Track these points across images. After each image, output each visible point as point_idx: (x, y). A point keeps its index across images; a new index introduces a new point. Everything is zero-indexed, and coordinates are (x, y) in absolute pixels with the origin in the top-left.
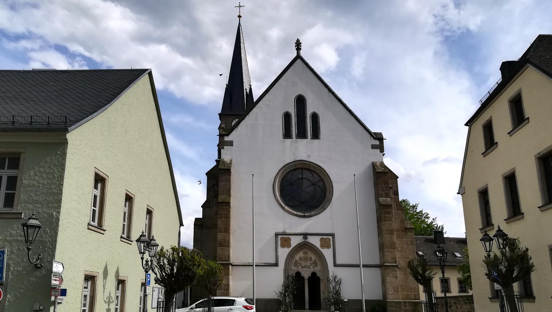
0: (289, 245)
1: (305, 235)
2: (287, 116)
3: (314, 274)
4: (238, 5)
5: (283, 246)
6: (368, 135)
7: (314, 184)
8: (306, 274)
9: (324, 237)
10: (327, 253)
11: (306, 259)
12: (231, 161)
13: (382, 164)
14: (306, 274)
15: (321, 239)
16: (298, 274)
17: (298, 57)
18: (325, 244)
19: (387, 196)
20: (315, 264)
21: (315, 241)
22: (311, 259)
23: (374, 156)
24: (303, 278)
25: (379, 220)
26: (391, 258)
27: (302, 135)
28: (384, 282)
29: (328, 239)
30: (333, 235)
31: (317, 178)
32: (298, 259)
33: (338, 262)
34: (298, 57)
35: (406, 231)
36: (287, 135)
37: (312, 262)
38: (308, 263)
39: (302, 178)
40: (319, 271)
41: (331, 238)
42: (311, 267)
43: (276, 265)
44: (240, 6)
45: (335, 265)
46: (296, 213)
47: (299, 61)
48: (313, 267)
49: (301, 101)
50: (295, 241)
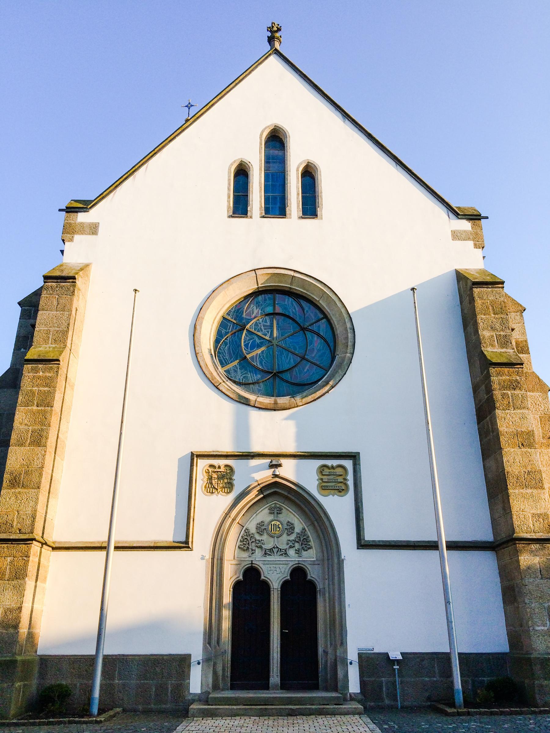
2: (242, 173)
3: (298, 572)
5: (211, 488)
8: (275, 574)
10: (338, 509)
14: (275, 574)
22: (290, 528)
24: (265, 586)
27: (276, 207)
29: (341, 468)
30: (354, 457)
31: (311, 314)
33: (369, 536)
36: (240, 207)
37: (293, 537)
41: (348, 464)
42: (292, 552)
43: (185, 545)
48: (298, 552)
49: (276, 140)
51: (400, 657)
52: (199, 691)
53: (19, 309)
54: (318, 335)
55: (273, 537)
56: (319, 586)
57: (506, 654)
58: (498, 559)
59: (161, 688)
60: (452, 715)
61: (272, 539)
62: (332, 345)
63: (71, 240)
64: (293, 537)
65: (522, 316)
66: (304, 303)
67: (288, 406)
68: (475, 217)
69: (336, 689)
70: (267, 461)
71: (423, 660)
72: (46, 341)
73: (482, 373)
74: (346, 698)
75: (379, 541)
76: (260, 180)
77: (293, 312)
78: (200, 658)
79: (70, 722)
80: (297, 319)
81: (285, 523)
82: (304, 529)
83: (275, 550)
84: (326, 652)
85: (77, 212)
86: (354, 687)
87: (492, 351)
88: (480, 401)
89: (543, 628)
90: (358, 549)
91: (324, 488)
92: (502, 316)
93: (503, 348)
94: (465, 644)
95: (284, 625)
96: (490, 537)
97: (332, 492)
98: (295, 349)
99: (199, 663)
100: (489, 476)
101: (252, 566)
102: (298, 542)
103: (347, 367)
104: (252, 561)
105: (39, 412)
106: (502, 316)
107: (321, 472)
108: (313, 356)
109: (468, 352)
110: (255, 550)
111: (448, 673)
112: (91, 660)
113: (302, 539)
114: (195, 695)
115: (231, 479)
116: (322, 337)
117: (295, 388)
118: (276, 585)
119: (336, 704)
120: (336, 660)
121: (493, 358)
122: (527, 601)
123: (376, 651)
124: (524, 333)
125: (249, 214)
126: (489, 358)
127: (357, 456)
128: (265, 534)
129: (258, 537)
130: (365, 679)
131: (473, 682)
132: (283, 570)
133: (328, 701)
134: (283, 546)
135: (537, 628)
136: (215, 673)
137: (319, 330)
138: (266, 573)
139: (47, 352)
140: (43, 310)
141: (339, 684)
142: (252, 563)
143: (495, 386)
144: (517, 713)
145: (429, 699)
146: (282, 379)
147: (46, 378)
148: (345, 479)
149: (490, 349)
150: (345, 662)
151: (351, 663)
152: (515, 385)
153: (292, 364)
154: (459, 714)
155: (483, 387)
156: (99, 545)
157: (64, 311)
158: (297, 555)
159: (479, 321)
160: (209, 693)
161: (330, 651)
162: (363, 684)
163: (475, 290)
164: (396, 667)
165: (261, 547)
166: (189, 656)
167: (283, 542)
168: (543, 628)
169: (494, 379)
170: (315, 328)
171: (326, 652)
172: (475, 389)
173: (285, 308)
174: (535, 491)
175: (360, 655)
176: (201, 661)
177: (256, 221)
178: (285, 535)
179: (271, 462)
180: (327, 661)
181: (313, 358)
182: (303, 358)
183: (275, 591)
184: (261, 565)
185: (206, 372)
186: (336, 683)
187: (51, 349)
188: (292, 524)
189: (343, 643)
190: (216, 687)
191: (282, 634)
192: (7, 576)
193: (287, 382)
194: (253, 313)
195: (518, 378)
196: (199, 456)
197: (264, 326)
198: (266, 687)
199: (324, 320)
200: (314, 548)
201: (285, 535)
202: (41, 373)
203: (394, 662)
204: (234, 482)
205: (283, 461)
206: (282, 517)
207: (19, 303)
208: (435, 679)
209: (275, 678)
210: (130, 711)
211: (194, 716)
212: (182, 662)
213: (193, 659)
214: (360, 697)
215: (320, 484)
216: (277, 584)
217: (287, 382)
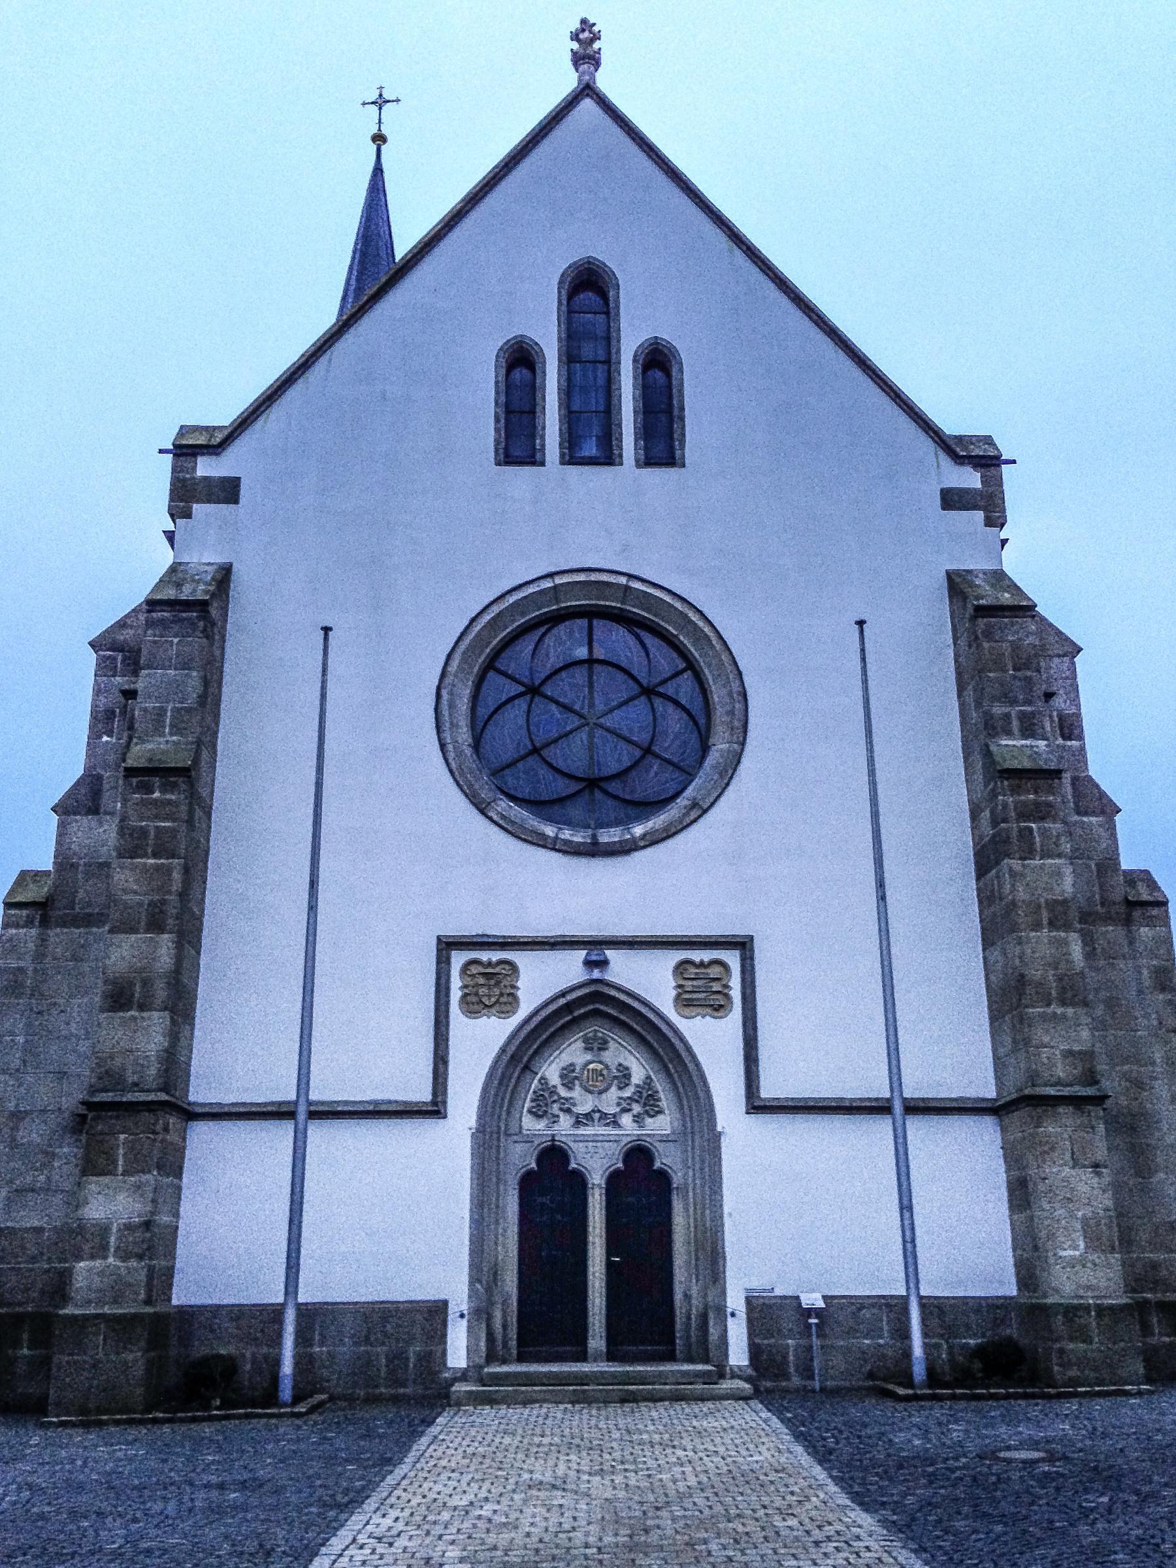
0: (507, 1002)
1: (596, 948)
2: (520, 358)
3: (638, 1156)
4: (374, 97)
5: (474, 1005)
6: (926, 446)
7: (649, 692)
8: (596, 1160)
9: (697, 956)
10: (712, 1041)
11: (598, 1082)
12: (224, 575)
13: (999, 578)
14: (596, 1160)
15: (681, 968)
16: (554, 1156)
17: (587, 90)
18: (701, 993)
19: (1029, 729)
20: (648, 1101)
21: (651, 980)
22: (624, 1076)
23: (960, 543)
24: (578, 1181)
25: (987, 858)
26: (1069, 1054)
27: (591, 443)
28: (1021, 1194)
29: (718, 967)
30: (744, 945)
31: (665, 660)
32: (554, 1079)
33: (768, 1090)
34: (587, 90)
35: (1128, 922)
36: (517, 444)
37: (628, 1093)
38: (610, 1101)
39: (591, 662)
40: (665, 1140)
41: (732, 959)
42: (626, 1120)
43: (435, 1110)
44: (381, 102)
45: (756, 1105)
46: (550, 831)
47: (587, 104)
48: (638, 1119)
49: (589, 286)
50: (541, 980)
51: (821, 1304)
52: (463, 1364)
53: (92, 657)
54: (677, 703)
55: (591, 1092)
56: (677, 1179)
57: (1011, 1298)
58: (1004, 1130)
59: (397, 1358)
60: (907, 1399)
61: (590, 1096)
62: (702, 721)
64: (628, 1093)
66: (649, 639)
69: (706, 1361)
70: (582, 954)
71: (860, 1309)
72: (158, 730)
73: (986, 786)
74: (721, 1372)
75: (787, 1099)
78: (464, 1307)
79: (247, 1416)
80: (635, 672)
82: (648, 1077)
84: (687, 1297)
86: (738, 1355)
88: (981, 837)
89: (1071, 1253)
90: (747, 1113)
91: (685, 1002)
92: (1029, 673)
95: (612, 1246)
96: (990, 1092)
97: (699, 1010)
99: (462, 1316)
100: (993, 978)
101: (553, 1145)
102: (637, 1101)
103: (730, 772)
104: (553, 1136)
105: (157, 868)
106: (1029, 673)
108: (668, 747)
110: (558, 1116)
111: (904, 1334)
112: (275, 1314)
113: (645, 1095)
116: (684, 708)
117: (631, 811)
118: (597, 1179)
119: (705, 1383)
124: (1076, 701)
125: (538, 456)
127: (748, 946)
128: (577, 1088)
129: (563, 1092)
130: (757, 1341)
131: (950, 1347)
135: (1064, 1253)
137: (677, 693)
138: (579, 1156)
142: (553, 1140)
144: (1017, 1396)
145: (871, 1375)
146: (606, 792)
148: (726, 986)
150: (721, 1311)
151: (733, 1315)
153: (627, 763)
154: (916, 1398)
155: (987, 813)
158: (635, 1125)
160: (481, 1367)
161: (694, 1291)
162: (755, 1352)
164: (813, 1321)
165: (568, 1111)
166: (445, 1303)
167: (610, 1101)
168: (1071, 1253)
170: (669, 689)
171: (687, 1297)
175: (749, 1301)
176: (465, 1312)
177: (555, 481)
178: (614, 1089)
181: (666, 749)
183: (597, 1192)
184: (572, 1144)
186: (707, 1348)
188: (627, 1069)
191: (610, 1265)
192: (120, 1169)
193: (616, 797)
198: (582, 1357)
199: (688, 675)
200: (667, 1112)
203: (809, 1312)
204: (520, 994)
206: (607, 1056)
207: (92, 644)
208: (881, 1341)
209: (597, 1341)
210: (344, 1398)
211: (459, 1404)
212: (435, 1314)
213: (453, 1310)
214: (750, 1371)
215: (678, 996)
216: (599, 1177)
217: (616, 797)
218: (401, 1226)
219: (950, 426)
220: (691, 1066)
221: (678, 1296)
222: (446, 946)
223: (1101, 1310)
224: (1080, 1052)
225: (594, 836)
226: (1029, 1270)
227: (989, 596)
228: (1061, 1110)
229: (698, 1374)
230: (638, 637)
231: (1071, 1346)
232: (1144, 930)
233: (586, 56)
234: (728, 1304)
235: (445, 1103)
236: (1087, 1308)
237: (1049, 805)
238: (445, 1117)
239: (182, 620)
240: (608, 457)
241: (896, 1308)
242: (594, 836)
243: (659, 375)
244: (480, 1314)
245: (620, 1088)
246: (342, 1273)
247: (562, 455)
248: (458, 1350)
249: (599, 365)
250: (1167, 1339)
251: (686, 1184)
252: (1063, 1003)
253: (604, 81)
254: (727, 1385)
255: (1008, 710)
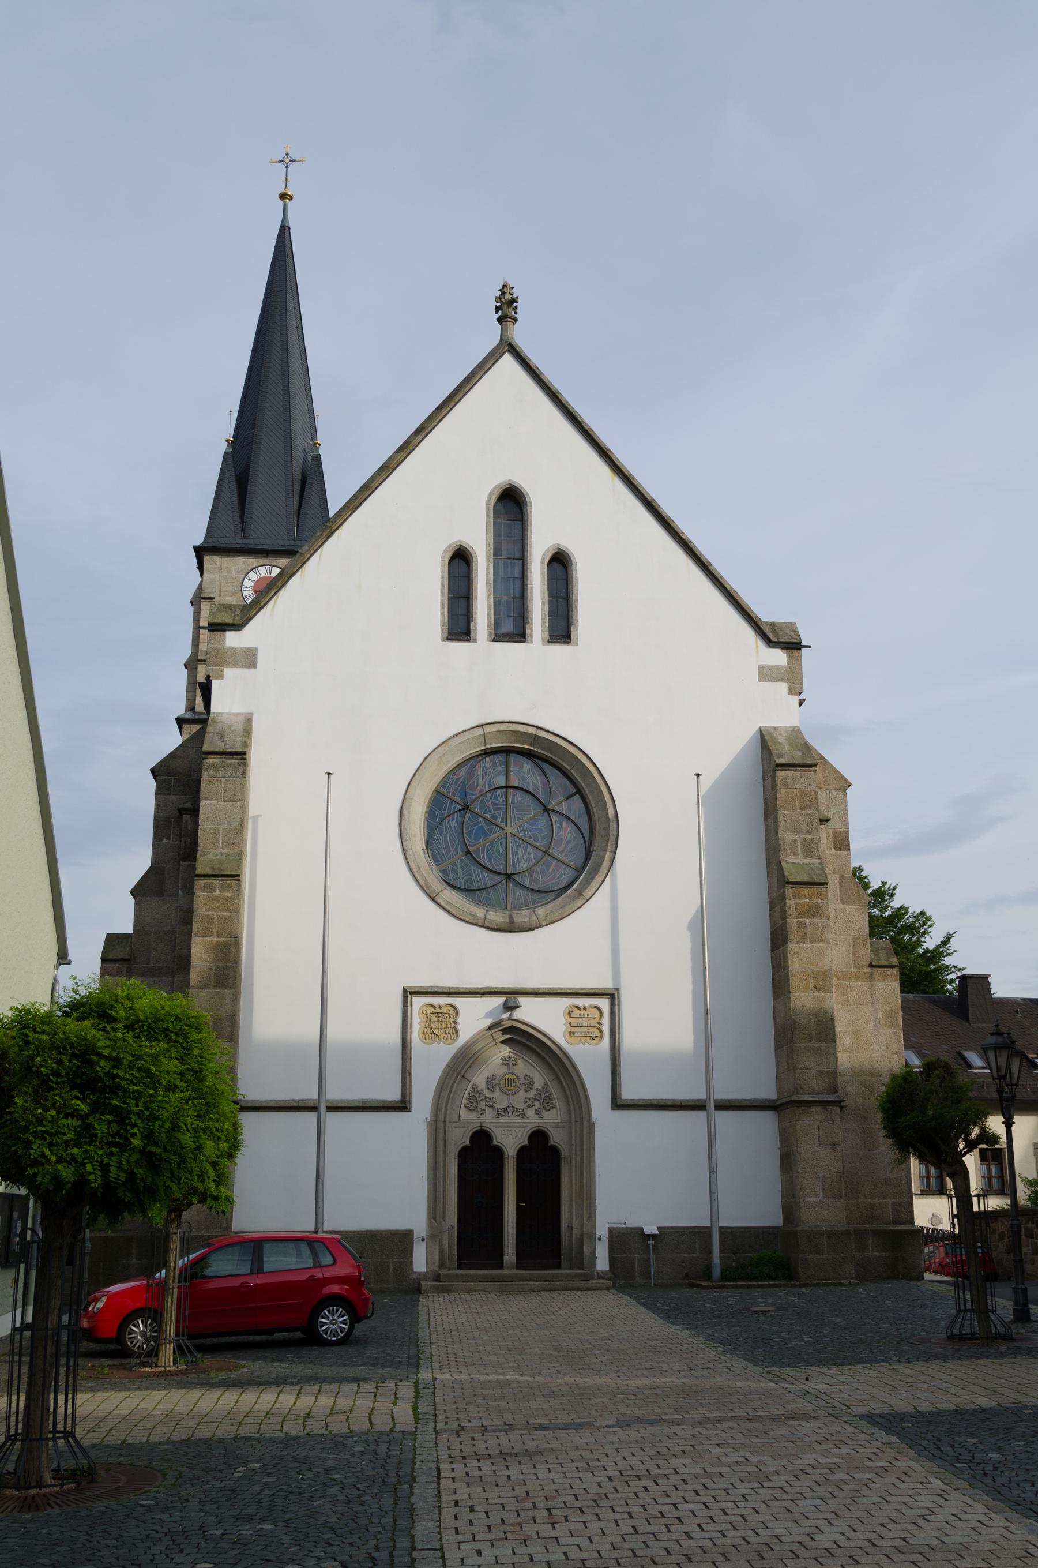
1: (511, 997)
2: (460, 559)
3: (539, 1136)
4: (282, 166)
8: (510, 1139)
9: (581, 1002)
14: (510, 1139)
16: (481, 1137)
22: (529, 1084)
24: (498, 1153)
26: (821, 1073)
27: (513, 629)
28: (788, 1161)
33: (627, 1094)
36: (459, 628)
37: (532, 1094)
41: (604, 1003)
42: (530, 1112)
43: (403, 1106)
44: (287, 161)
45: (618, 1104)
48: (538, 1112)
49: (511, 503)
51: (656, 1232)
52: (423, 1269)
56: (564, 1152)
58: (780, 1121)
60: (708, 1288)
63: (220, 676)
65: (845, 795)
66: (546, 767)
67: (527, 926)
68: (793, 646)
76: (488, 579)
77: (534, 785)
78: (424, 1234)
81: (522, 1077)
82: (546, 1084)
83: (510, 1110)
84: (570, 1228)
85: (225, 631)
86: (602, 1264)
87: (793, 862)
92: (810, 812)
93: (806, 857)
94: (731, 1218)
95: (519, 1198)
98: (536, 839)
99: (423, 1240)
106: (810, 812)
107: (569, 1014)
109: (767, 850)
111: (708, 1250)
114: (420, 1274)
115: (455, 1022)
117: (536, 896)
118: (511, 1151)
120: (582, 1235)
121: (791, 874)
122: (800, 1170)
123: (629, 1225)
124: (846, 821)
125: (472, 634)
126: (786, 873)
128: (497, 1090)
129: (487, 1094)
130: (616, 1256)
132: (520, 1135)
133: (575, 1277)
134: (520, 1106)
135: (809, 1200)
136: (441, 1251)
139: (221, 862)
140: (206, 799)
141: (586, 1263)
143: (791, 912)
145: (687, 1276)
147: (226, 899)
149: (792, 859)
150: (592, 1236)
151: (600, 1239)
152: (815, 911)
156: (294, 1104)
157: (234, 800)
159: (781, 818)
161: (575, 1224)
162: (612, 1260)
163: (779, 773)
165: (492, 1107)
167: (519, 1100)
169: (791, 902)
172: (772, 906)
173: (523, 778)
174: (824, 1046)
175: (610, 1231)
177: (481, 647)
178: (522, 1092)
179: (506, 1002)
180: (571, 1236)
182: (546, 852)
185: (419, 878)
186: (582, 1261)
187: (224, 857)
189: (592, 1217)
190: (442, 1266)
191: (518, 1208)
194: (478, 785)
195: (820, 902)
196: (412, 993)
197: (493, 804)
198: (501, 1266)
199: (578, 796)
201: (522, 1092)
202: (218, 893)
203: (649, 1237)
205: (522, 1000)
209: (510, 1255)
212: (403, 1239)
213: (417, 1235)
214: (610, 1275)
218: (385, 1183)
219: (765, 615)
220: (576, 1079)
221: (564, 1225)
222: (407, 994)
223: (831, 1235)
224: (828, 1072)
225: (511, 917)
226: (789, 1210)
227: (787, 753)
228: (813, 1109)
229: (576, 1275)
230: (536, 764)
231: (811, 1256)
232: (881, 985)
233: (506, 307)
234: (597, 1232)
235: (410, 1102)
236: (821, 1233)
237: (817, 906)
238: (410, 1111)
239: (227, 765)
240: (520, 635)
241: (703, 1233)
242: (511, 917)
243: (560, 568)
244: (433, 1237)
245: (527, 1092)
246: (352, 1212)
247: (490, 635)
248: (421, 1260)
249: (516, 561)
250: (877, 1254)
251: (570, 1155)
252: (819, 1040)
253: (519, 334)
254: (593, 1282)
255: (795, 837)
